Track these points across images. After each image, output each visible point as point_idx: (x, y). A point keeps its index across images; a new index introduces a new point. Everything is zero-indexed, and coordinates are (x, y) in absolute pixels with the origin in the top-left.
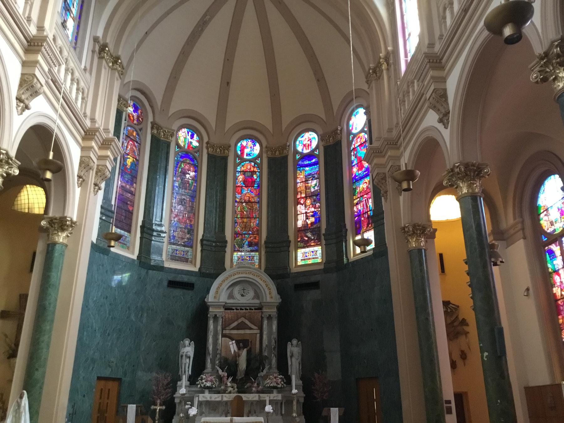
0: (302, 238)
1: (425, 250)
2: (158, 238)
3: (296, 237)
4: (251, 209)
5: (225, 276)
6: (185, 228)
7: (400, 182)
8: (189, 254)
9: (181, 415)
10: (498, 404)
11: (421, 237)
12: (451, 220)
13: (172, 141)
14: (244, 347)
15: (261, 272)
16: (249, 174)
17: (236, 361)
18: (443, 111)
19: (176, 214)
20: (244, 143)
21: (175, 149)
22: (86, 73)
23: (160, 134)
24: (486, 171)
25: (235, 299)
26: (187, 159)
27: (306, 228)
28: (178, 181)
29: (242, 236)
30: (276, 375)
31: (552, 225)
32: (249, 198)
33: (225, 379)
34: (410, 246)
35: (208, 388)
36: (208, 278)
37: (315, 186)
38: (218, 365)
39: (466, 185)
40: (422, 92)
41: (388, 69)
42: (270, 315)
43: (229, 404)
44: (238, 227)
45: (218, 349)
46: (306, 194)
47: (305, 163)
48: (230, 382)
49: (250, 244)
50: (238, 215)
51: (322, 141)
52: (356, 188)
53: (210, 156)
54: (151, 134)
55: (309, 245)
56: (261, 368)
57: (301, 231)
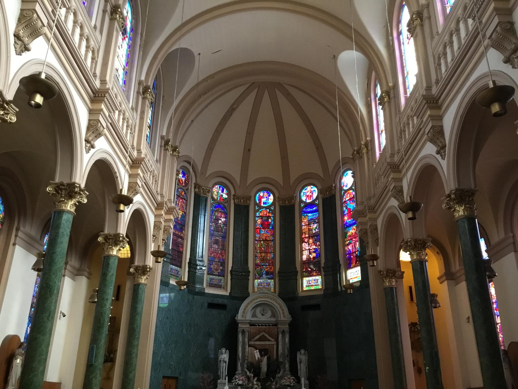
0: (306, 269)
3: (302, 268)
4: (268, 246)
8: (222, 281)
11: (392, 279)
16: (265, 218)
22: (157, 163)
33: (252, 379)
37: (316, 229)
39: (416, 253)
41: (367, 153)
44: (258, 259)
45: (245, 356)
47: (308, 210)
56: (278, 371)
57: (306, 263)
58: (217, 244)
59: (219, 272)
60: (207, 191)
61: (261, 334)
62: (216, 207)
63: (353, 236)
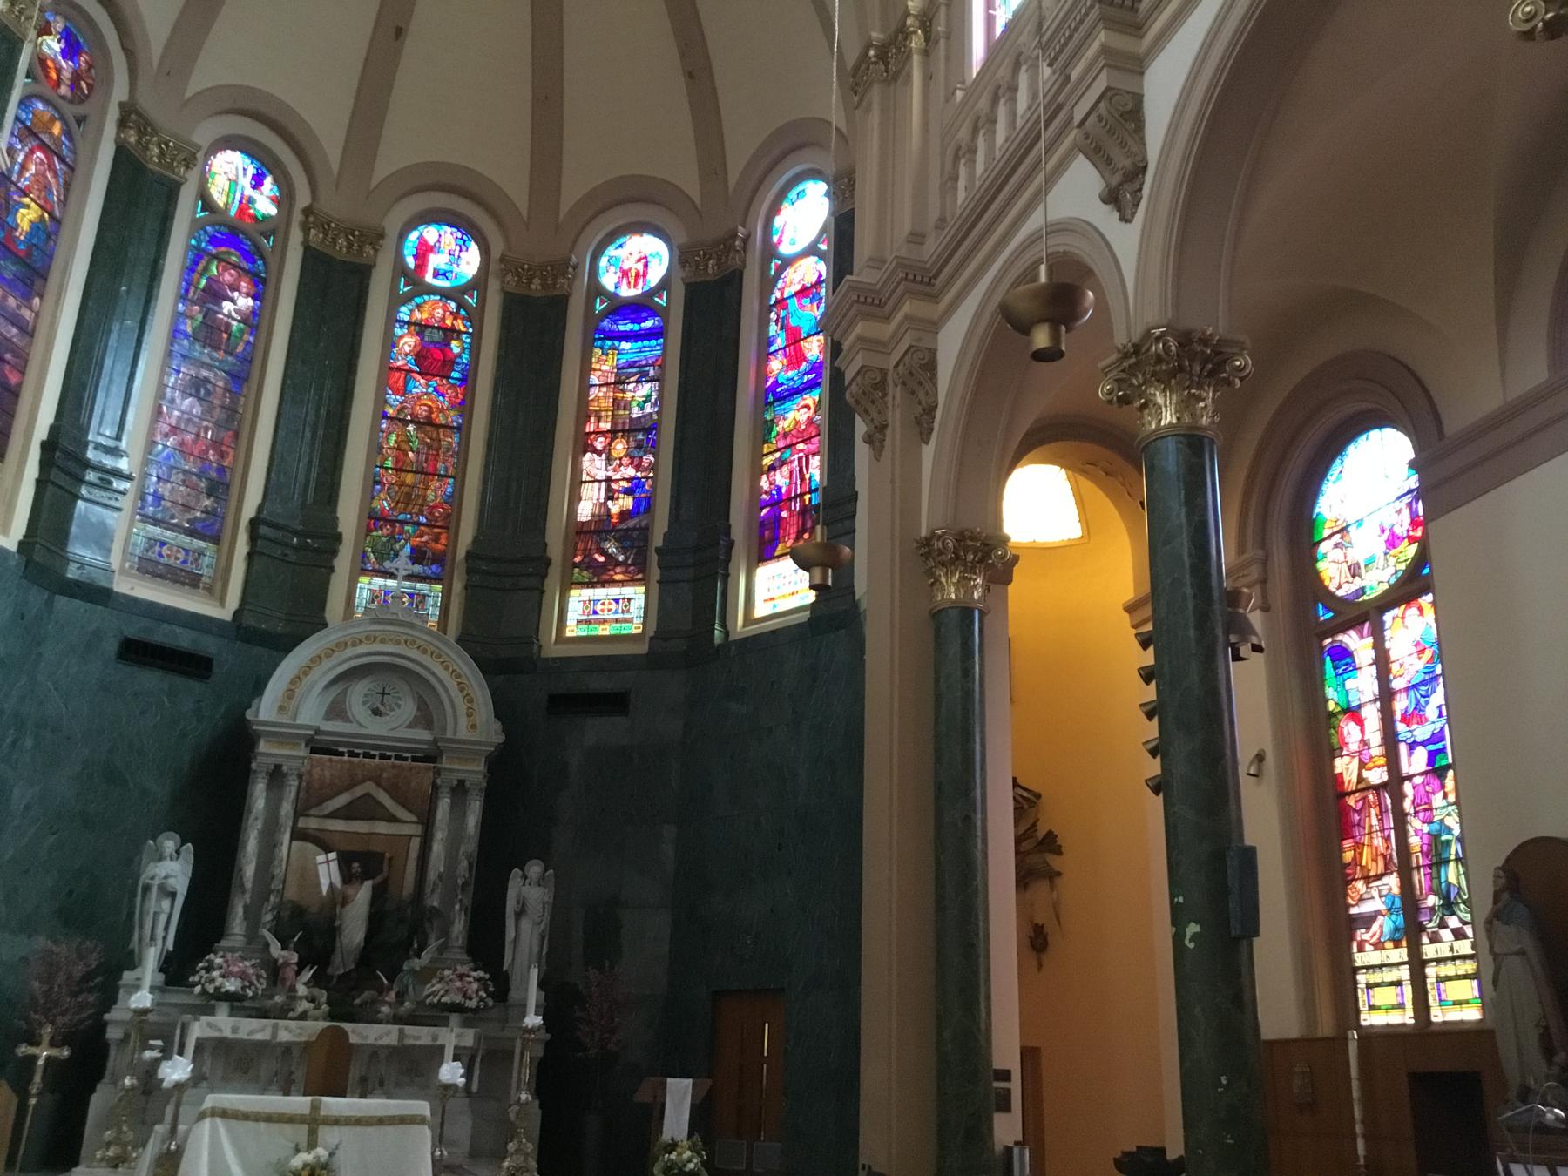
0: (587, 555)
1: (982, 613)
2: (103, 494)
3: (570, 550)
4: (433, 449)
5: (323, 642)
6: (199, 476)
7: (1025, 329)
8: (206, 561)
9: (127, 1082)
10: (1219, 1090)
12: (1044, 543)
13: (186, 180)
14: (366, 875)
15: (446, 643)
16: (437, 336)
17: (333, 918)
18: (1123, 162)
19: (174, 423)
20: (431, 233)
21: (196, 213)
23: (147, 148)
24: (1238, 363)
25: (351, 722)
26: (233, 250)
27: (602, 526)
28: (192, 318)
29: (393, 526)
30: (462, 969)
31: (1353, 576)
32: (431, 411)
33: (289, 973)
34: (939, 598)
35: (229, 997)
36: (260, 645)
37: (645, 402)
38: (268, 926)
40: (1060, 99)
41: (926, 53)
42: (461, 783)
43: (296, 1052)
44: (382, 495)
46: (614, 423)
47: (622, 328)
48: (305, 984)
49: (418, 556)
50: (386, 459)
51: (684, 267)
52: (772, 420)
53: (312, 257)
54: (116, 142)
55: (606, 577)
56: (416, 946)
57: (586, 533)
58: (199, 399)
59: (196, 519)
60: (181, 157)
61: (359, 791)
62: (213, 241)
63: (801, 435)
